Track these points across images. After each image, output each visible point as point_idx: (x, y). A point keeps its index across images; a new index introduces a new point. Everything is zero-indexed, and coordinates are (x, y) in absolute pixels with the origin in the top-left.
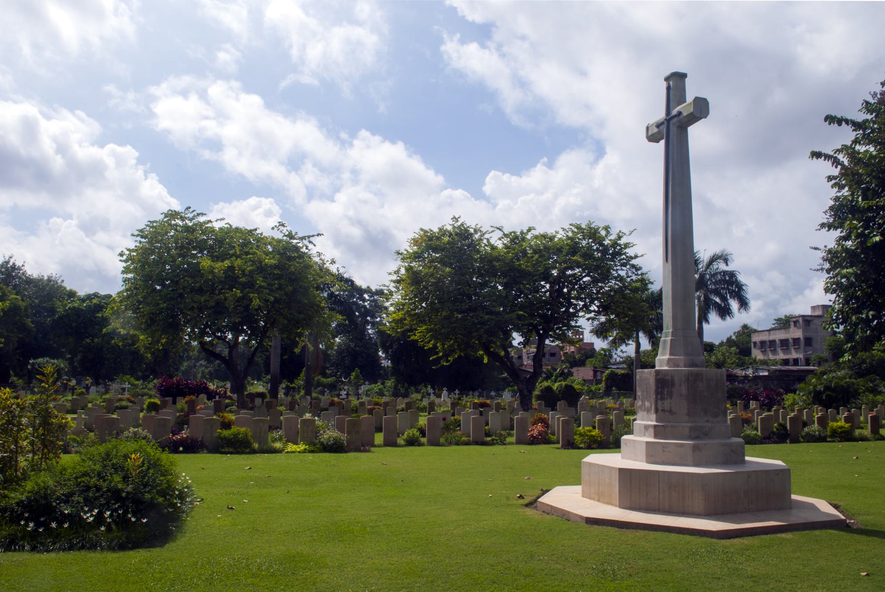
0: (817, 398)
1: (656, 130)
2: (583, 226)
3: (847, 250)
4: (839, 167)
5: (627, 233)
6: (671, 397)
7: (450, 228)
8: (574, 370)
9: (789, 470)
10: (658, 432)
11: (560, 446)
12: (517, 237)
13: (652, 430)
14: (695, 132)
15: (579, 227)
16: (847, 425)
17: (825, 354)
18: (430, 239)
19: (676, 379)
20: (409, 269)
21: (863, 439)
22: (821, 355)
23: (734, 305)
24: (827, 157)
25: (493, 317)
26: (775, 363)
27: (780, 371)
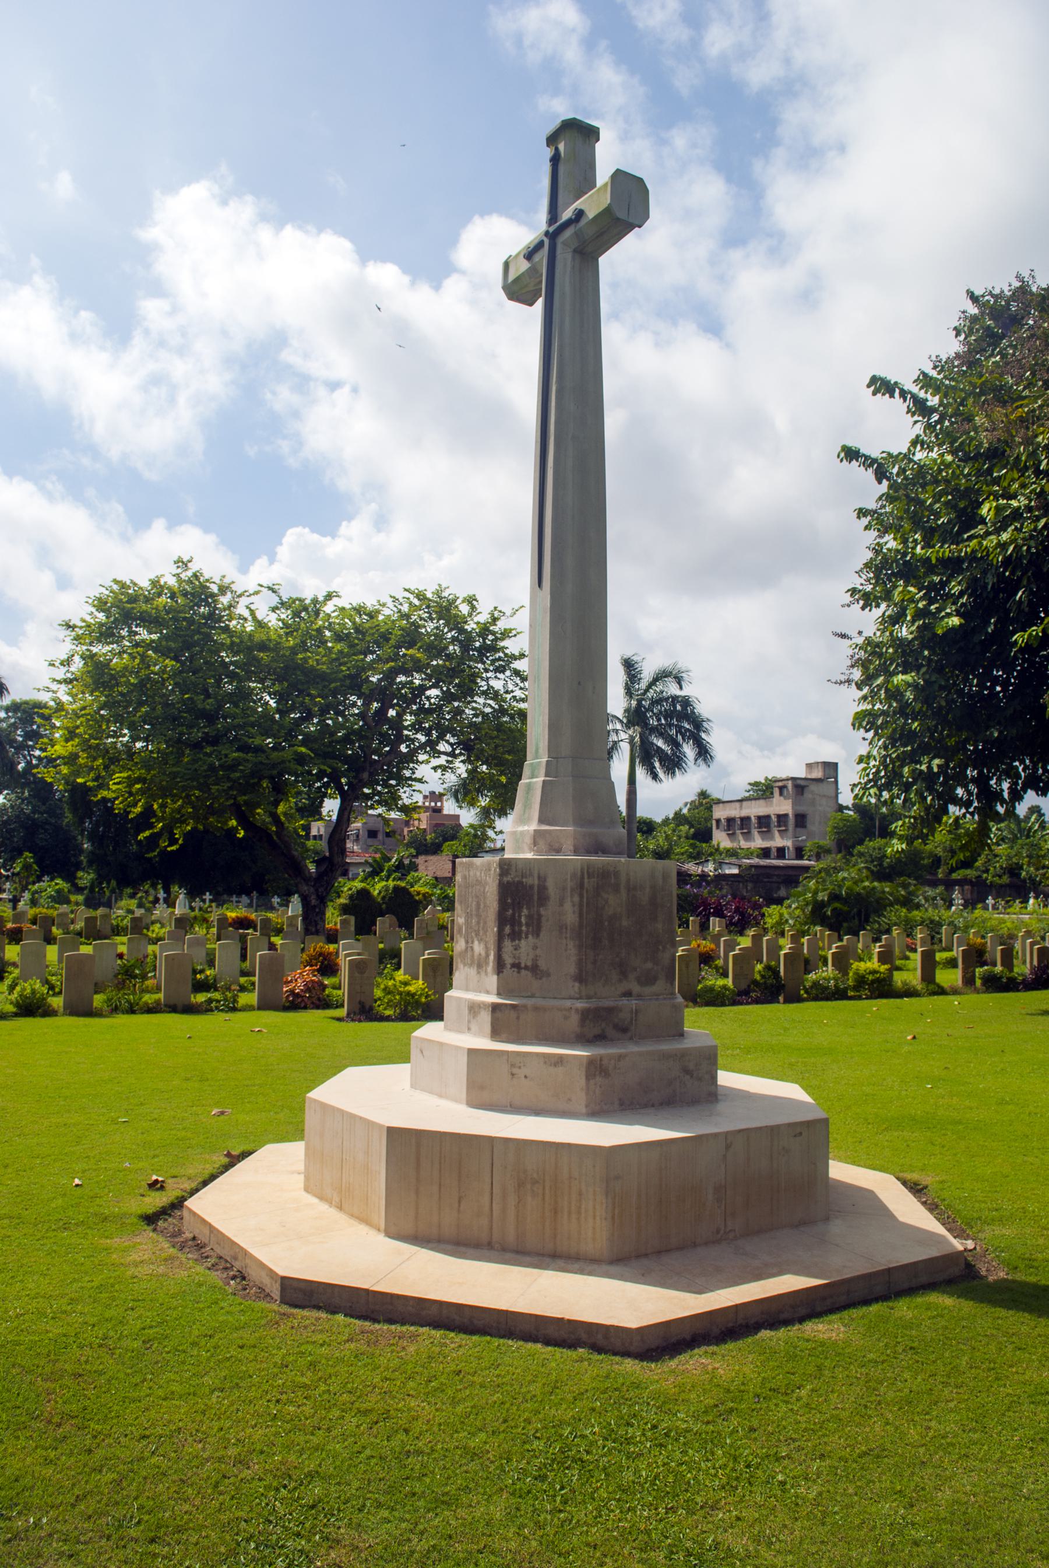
0: (818, 914)
1: (524, 266)
2: (429, 595)
3: (899, 644)
4: (885, 483)
5: (508, 613)
6: (537, 933)
7: (172, 582)
8: (420, 860)
9: (825, 1122)
10: (503, 1022)
11: (342, 1012)
12: (305, 609)
13: (486, 1017)
14: (616, 263)
15: (421, 596)
16: (883, 968)
17: (827, 842)
18: (133, 599)
19: (550, 884)
20: (89, 658)
21: (909, 993)
22: (822, 843)
23: (689, 750)
24: (868, 462)
25: (250, 756)
26: (749, 854)
27: (757, 867)
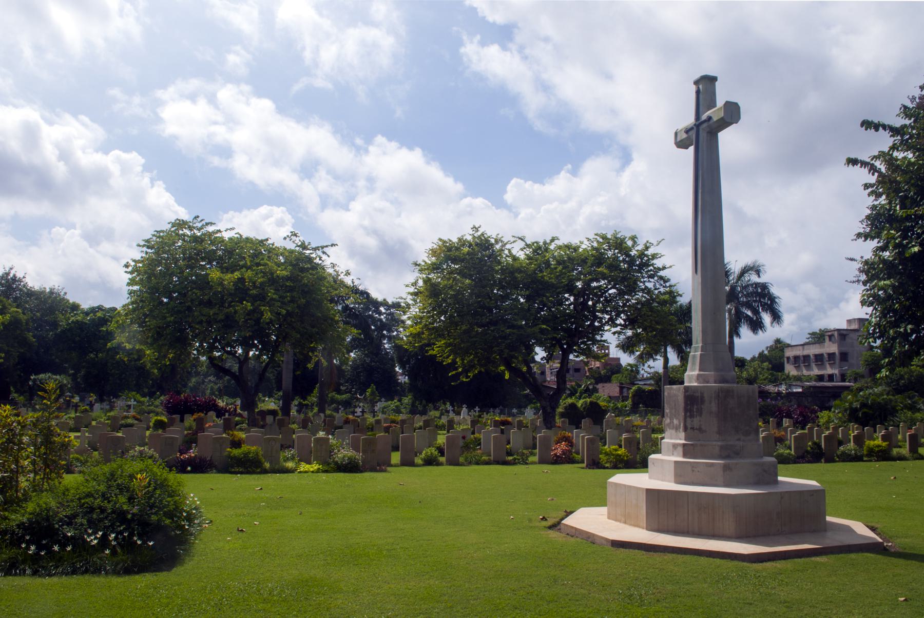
0: (853, 415)
1: (685, 136)
2: (609, 236)
3: (884, 261)
4: (876, 174)
5: (655, 243)
6: (701, 415)
7: (469, 238)
8: (599, 386)
9: (824, 491)
10: (687, 451)
11: (584, 465)
12: (540, 248)
13: (680, 449)
14: (726, 138)
15: (604, 237)
16: (884, 444)
17: (862, 370)
18: (449, 249)
19: (705, 395)
20: (427, 281)
21: (901, 458)
22: (858, 371)
23: (766, 318)
24: (864, 164)
25: (515, 331)
26: (809, 379)
27: (814, 387)
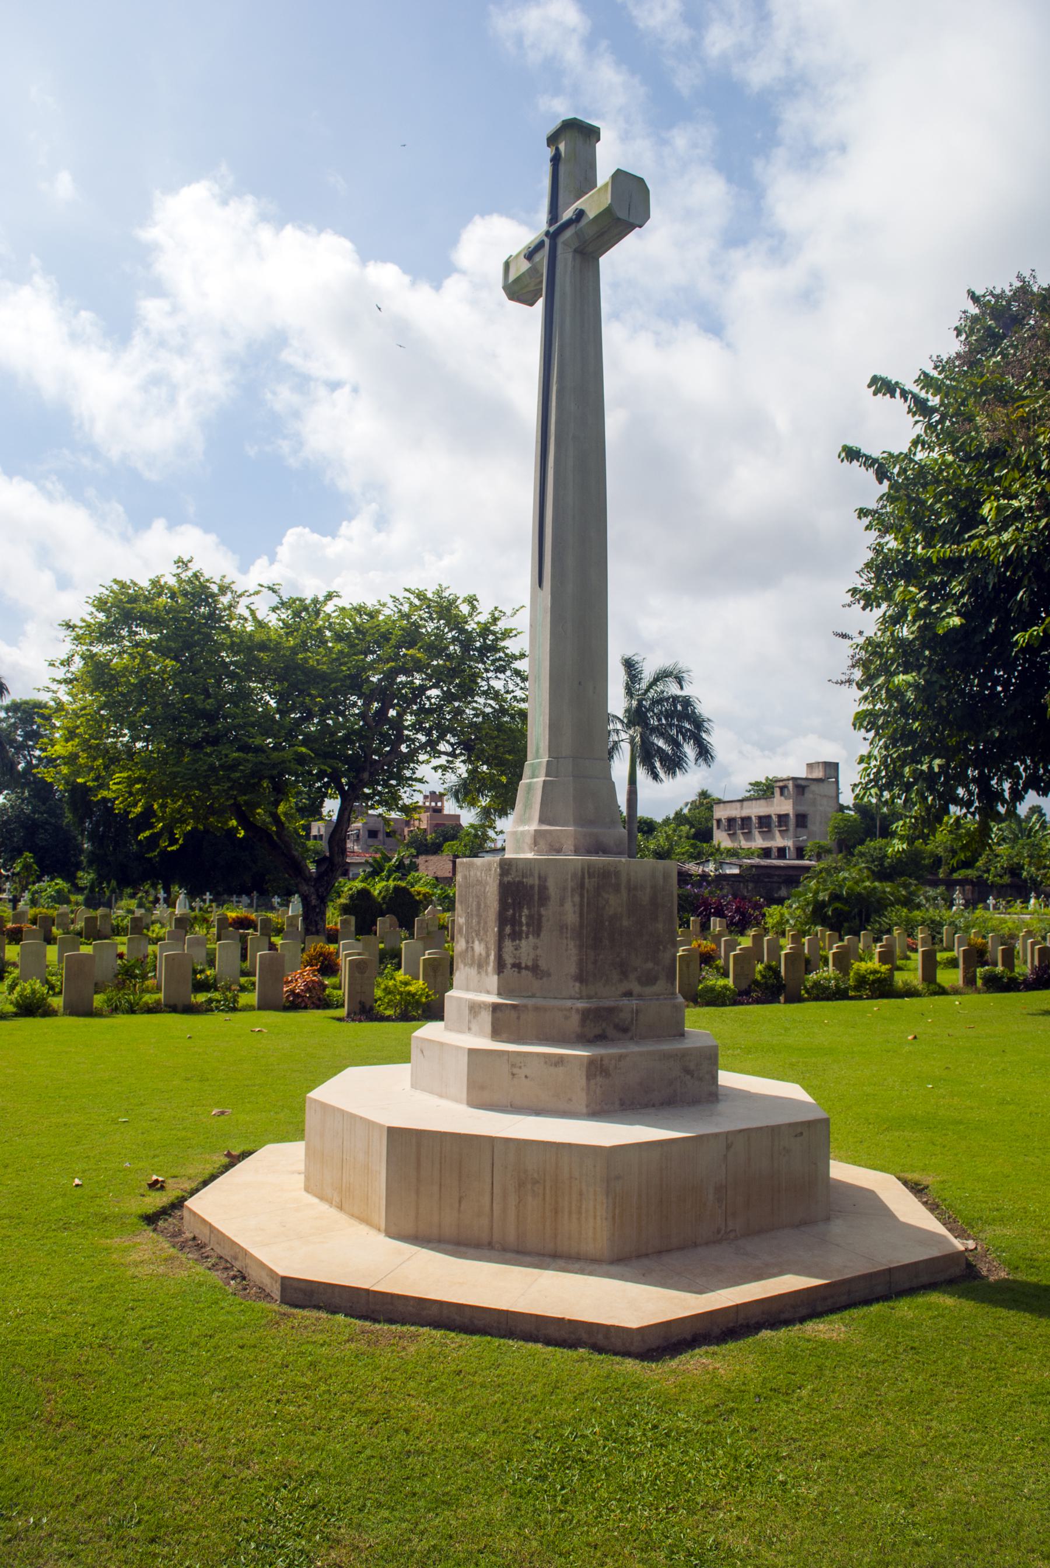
0: (818, 914)
1: (525, 266)
2: (430, 595)
3: (900, 644)
4: (886, 483)
5: (509, 613)
6: (538, 933)
7: (172, 582)
8: (421, 860)
9: (826, 1122)
10: (503, 1022)
11: (343, 1012)
12: (306, 609)
13: (486, 1017)
14: (617, 263)
15: (421, 596)
16: (884, 968)
17: (828, 842)
18: (133, 599)
19: (551, 884)
20: (89, 658)
21: (910, 993)
22: (823, 843)
23: (689, 750)
24: (869, 462)
25: (250, 756)
26: (750, 854)
27: (758, 867)
